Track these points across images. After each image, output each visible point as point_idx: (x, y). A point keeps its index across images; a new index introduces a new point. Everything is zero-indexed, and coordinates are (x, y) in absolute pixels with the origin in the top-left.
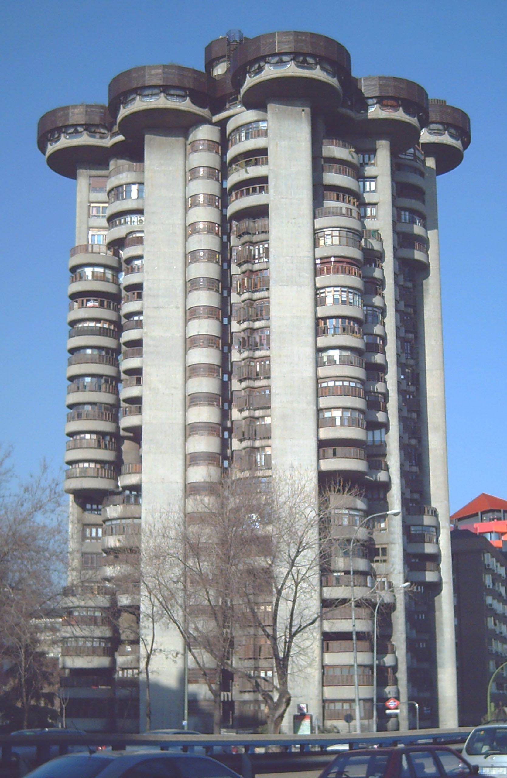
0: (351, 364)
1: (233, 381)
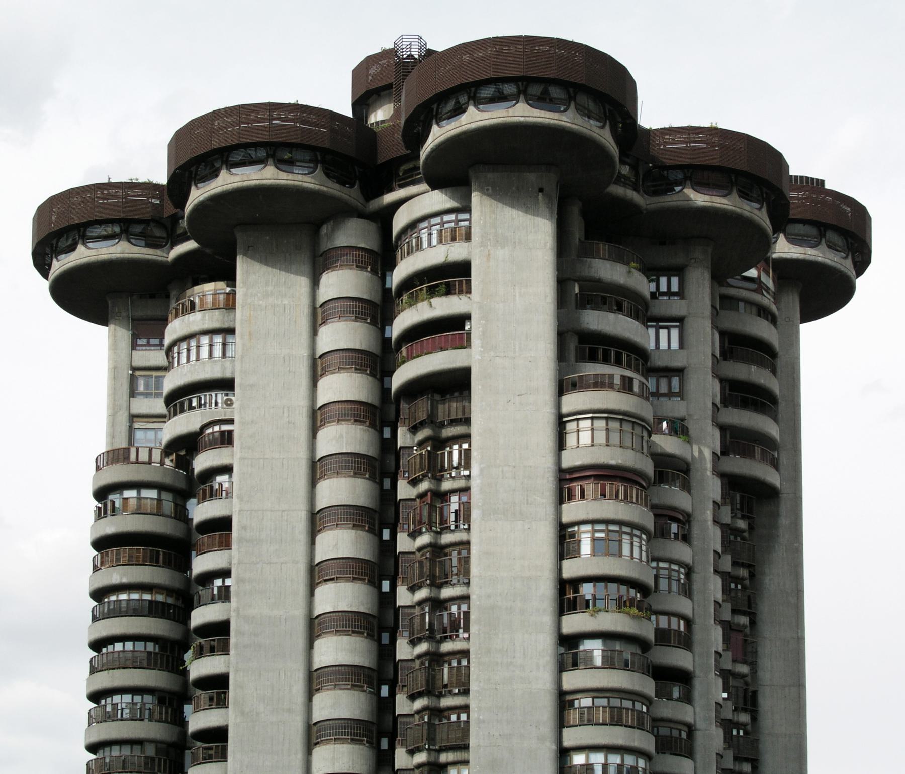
0: (626, 666)
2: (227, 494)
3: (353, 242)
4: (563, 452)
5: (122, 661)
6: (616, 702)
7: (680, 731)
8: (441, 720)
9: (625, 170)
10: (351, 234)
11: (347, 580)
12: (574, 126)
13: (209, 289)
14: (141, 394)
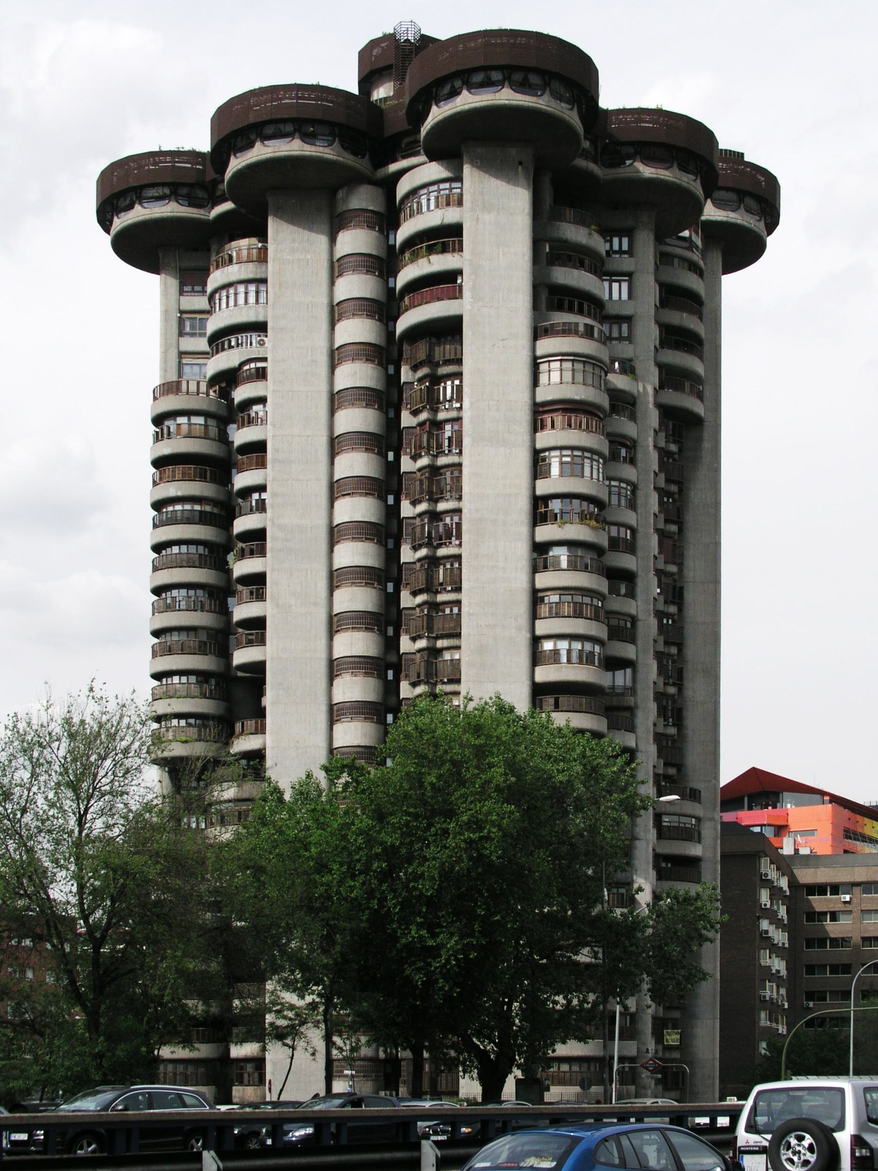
0: (585, 569)
1: (402, 593)
2: (262, 421)
3: (364, 205)
4: (537, 389)
5: (179, 561)
6: (578, 599)
7: (626, 621)
8: (437, 613)
9: (586, 144)
10: (363, 199)
11: (361, 494)
12: (549, 109)
13: (244, 245)
14: (188, 334)
